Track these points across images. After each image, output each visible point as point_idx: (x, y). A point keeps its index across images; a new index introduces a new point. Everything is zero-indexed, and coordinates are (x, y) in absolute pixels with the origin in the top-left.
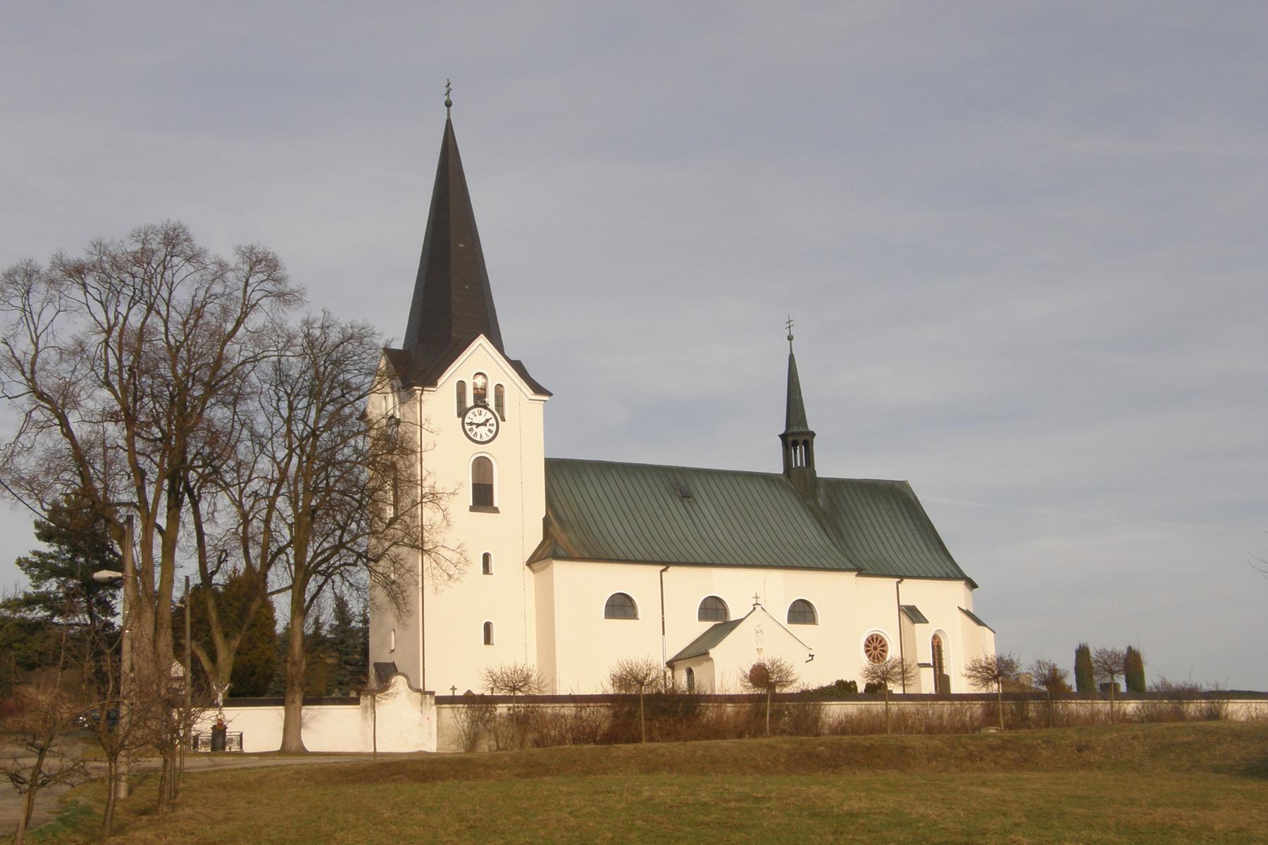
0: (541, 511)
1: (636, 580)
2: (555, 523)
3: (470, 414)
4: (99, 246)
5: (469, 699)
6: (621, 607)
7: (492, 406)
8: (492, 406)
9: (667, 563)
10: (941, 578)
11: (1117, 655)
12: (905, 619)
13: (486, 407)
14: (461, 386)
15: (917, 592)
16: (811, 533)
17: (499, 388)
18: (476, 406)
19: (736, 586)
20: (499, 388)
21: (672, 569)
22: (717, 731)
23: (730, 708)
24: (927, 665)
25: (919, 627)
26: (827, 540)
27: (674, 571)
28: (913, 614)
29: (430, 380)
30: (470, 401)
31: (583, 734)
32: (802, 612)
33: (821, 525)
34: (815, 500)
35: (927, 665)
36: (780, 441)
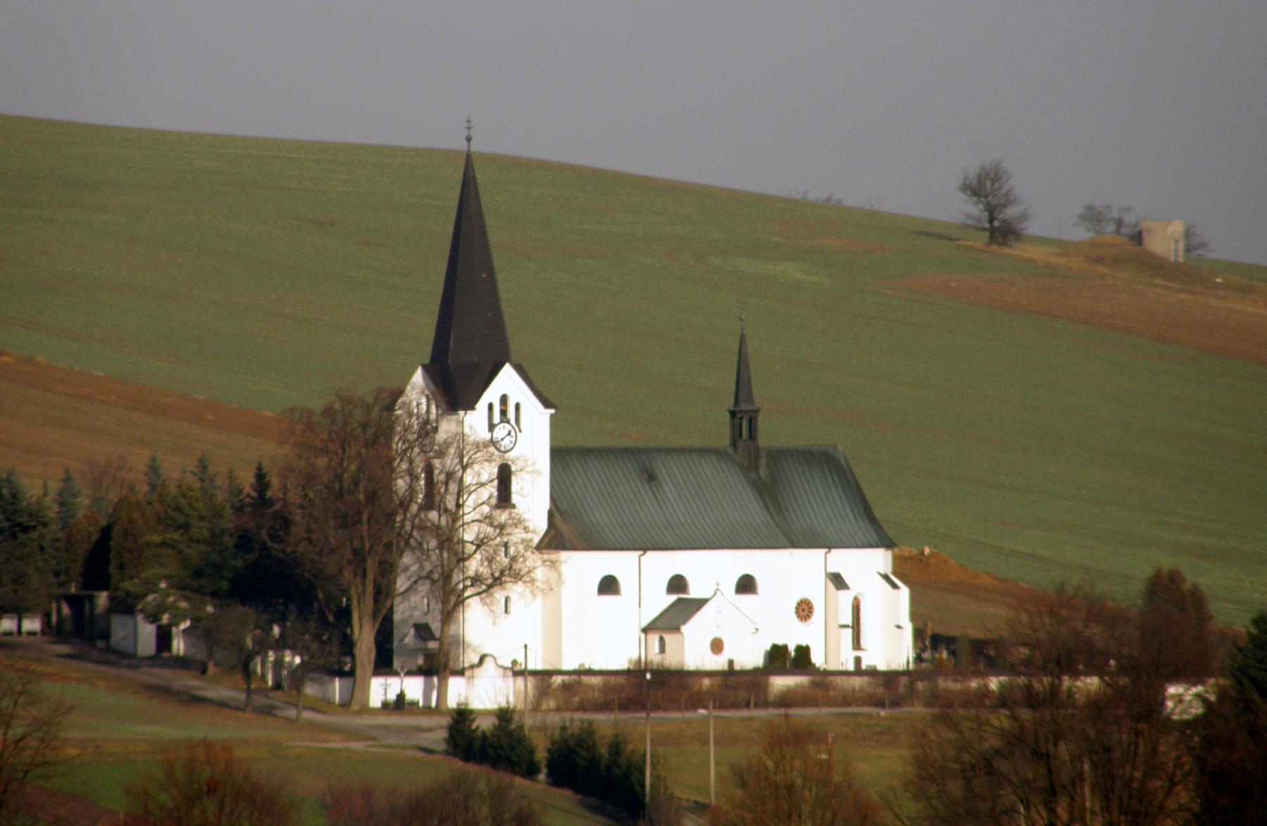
0: (546, 505)
1: (618, 563)
2: (557, 515)
3: (497, 429)
4: (1093, 216)
5: (534, 673)
6: (609, 586)
7: (513, 422)
8: (513, 422)
9: (645, 549)
10: (858, 547)
11: (1097, 611)
12: (831, 586)
13: (508, 422)
14: (491, 406)
15: (846, 560)
16: (754, 510)
17: (517, 407)
18: (502, 422)
19: (709, 570)
20: (517, 407)
21: (649, 554)
22: (696, 701)
23: (706, 682)
24: (847, 626)
25: (842, 593)
26: (769, 518)
27: (651, 555)
28: (838, 581)
29: (470, 406)
30: (497, 418)
31: (6, 612)
32: (746, 585)
33: (765, 503)
34: (757, 470)
35: (847, 626)
36: (728, 416)
